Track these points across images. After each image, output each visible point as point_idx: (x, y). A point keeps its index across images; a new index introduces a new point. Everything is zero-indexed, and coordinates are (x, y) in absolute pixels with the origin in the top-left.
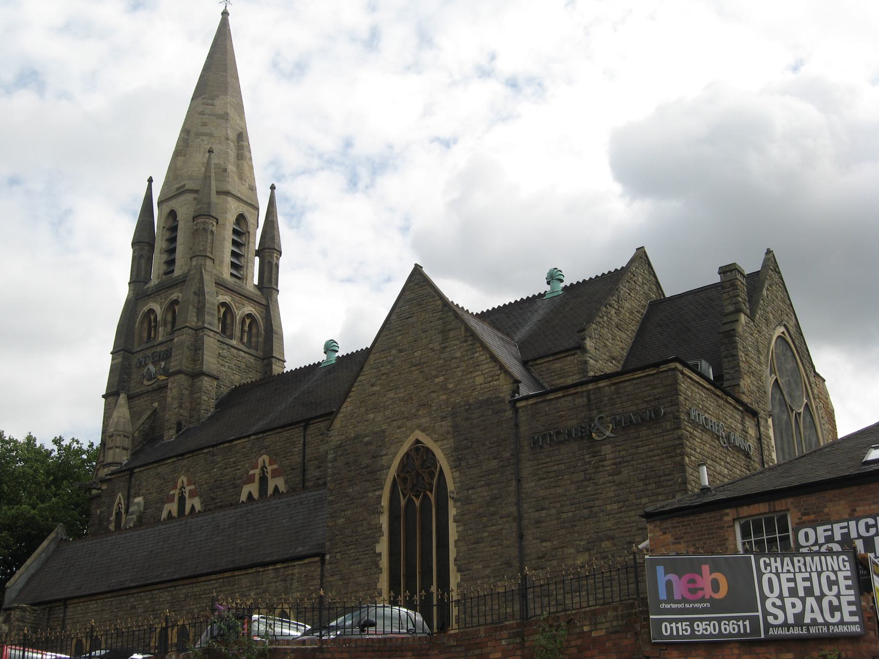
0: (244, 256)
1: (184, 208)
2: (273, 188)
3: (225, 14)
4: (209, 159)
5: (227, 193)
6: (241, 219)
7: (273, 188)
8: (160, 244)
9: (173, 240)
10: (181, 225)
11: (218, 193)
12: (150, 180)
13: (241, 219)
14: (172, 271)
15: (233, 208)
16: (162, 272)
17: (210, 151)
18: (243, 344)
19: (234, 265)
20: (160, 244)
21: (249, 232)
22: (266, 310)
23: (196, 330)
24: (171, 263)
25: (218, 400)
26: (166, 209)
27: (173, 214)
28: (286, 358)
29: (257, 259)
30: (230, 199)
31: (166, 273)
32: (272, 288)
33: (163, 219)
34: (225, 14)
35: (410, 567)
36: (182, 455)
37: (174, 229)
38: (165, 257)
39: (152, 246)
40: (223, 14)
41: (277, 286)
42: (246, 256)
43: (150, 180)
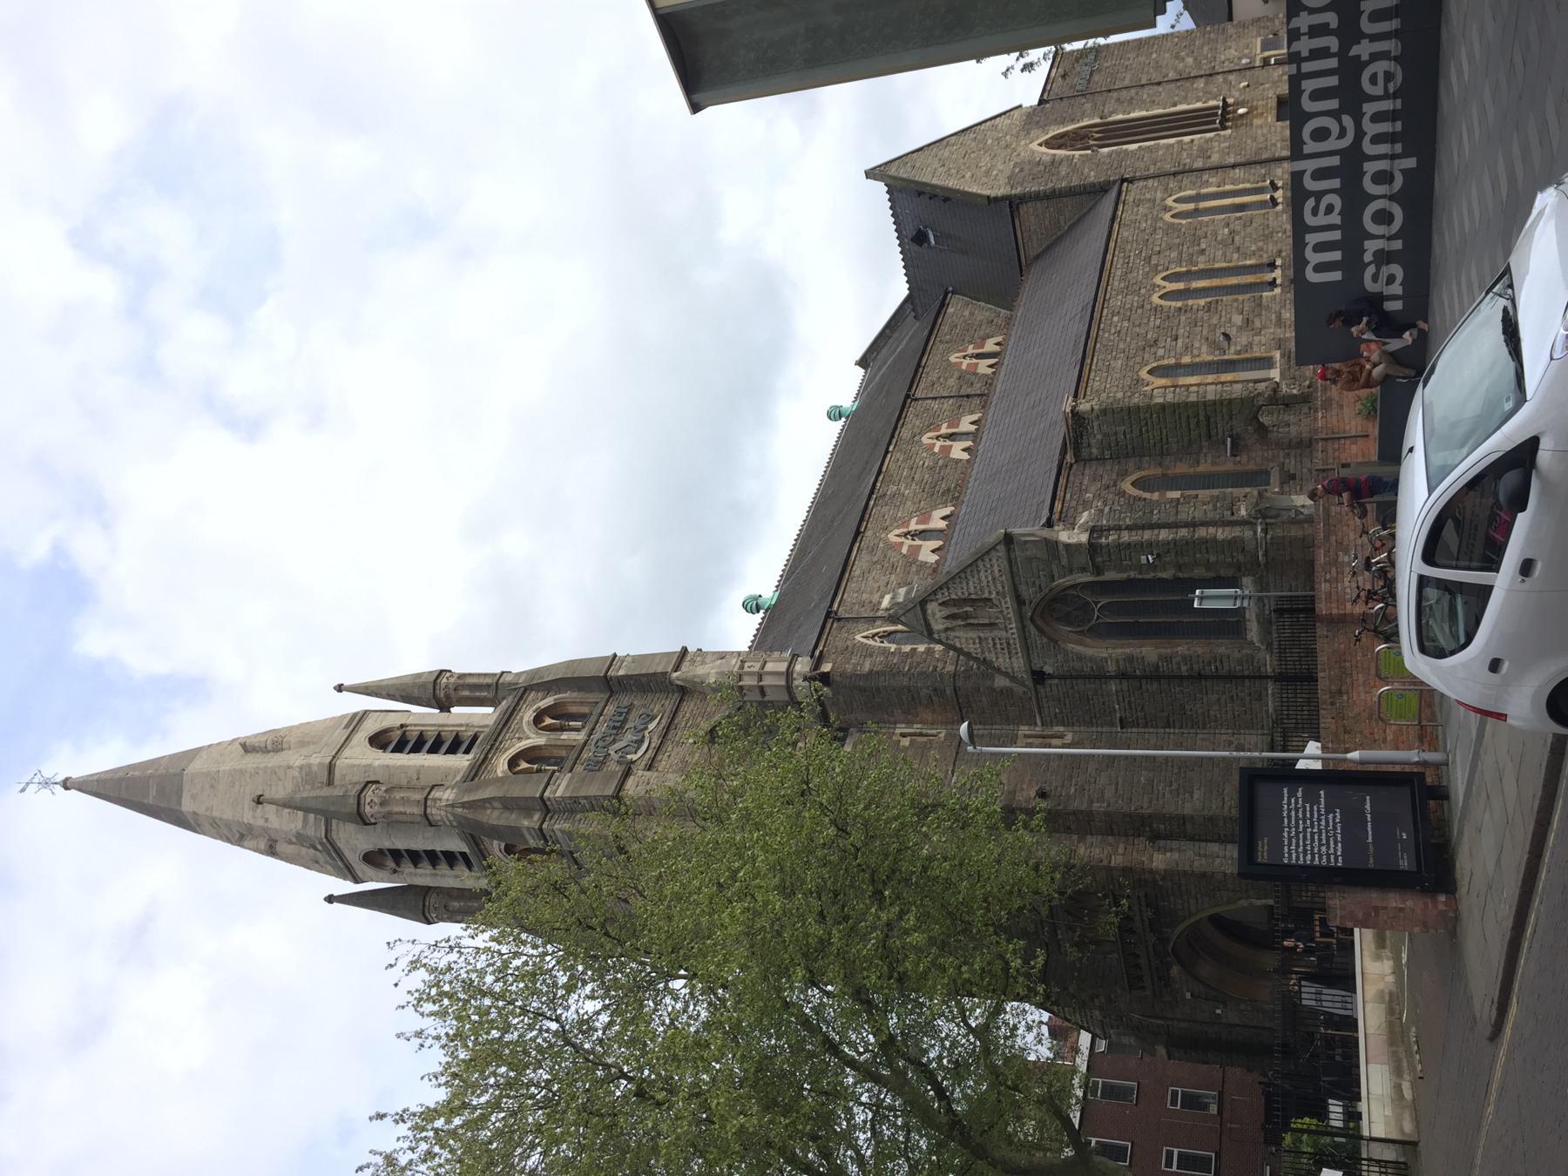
0: (422, 732)
1: (355, 841)
2: (340, 688)
3: (67, 784)
4: (272, 802)
5: (331, 767)
6: (379, 741)
7: (340, 688)
8: (422, 876)
9: (415, 857)
10: (387, 844)
11: (330, 782)
12: (330, 899)
13: (379, 741)
14: (463, 854)
15: (362, 757)
16: (467, 872)
17: (259, 801)
18: (583, 727)
19: (453, 750)
20: (422, 876)
21: (402, 726)
22: (532, 690)
23: (548, 811)
24: (451, 858)
25: (1293, 327)
26: (361, 868)
27: (374, 859)
28: (609, 653)
29: (455, 710)
30: (340, 763)
31: (469, 865)
32: (497, 683)
33: (381, 874)
34: (67, 784)
35: (1110, 130)
36: (858, 533)
37: (396, 855)
38: (443, 868)
39: (426, 891)
40: (66, 788)
41: (496, 675)
42: (441, 729)
43: (330, 899)
